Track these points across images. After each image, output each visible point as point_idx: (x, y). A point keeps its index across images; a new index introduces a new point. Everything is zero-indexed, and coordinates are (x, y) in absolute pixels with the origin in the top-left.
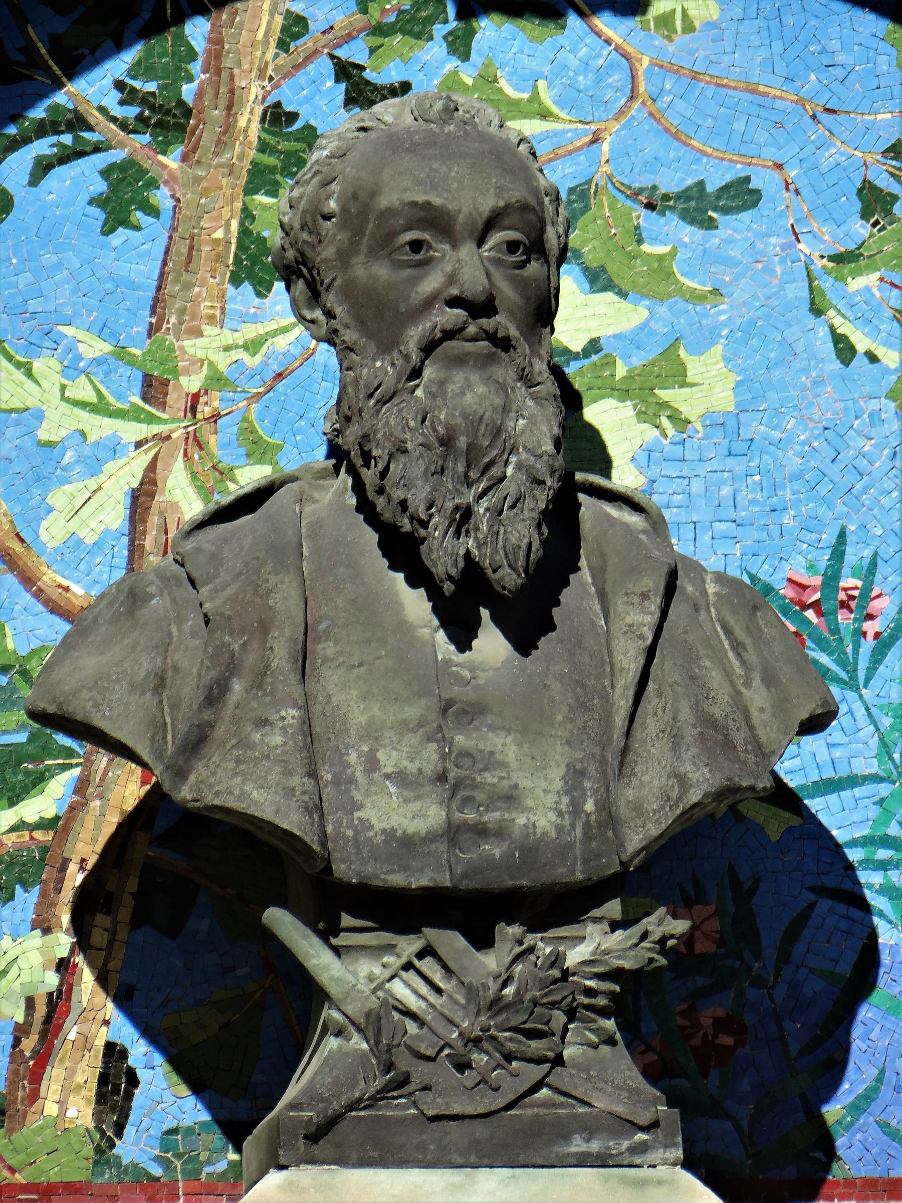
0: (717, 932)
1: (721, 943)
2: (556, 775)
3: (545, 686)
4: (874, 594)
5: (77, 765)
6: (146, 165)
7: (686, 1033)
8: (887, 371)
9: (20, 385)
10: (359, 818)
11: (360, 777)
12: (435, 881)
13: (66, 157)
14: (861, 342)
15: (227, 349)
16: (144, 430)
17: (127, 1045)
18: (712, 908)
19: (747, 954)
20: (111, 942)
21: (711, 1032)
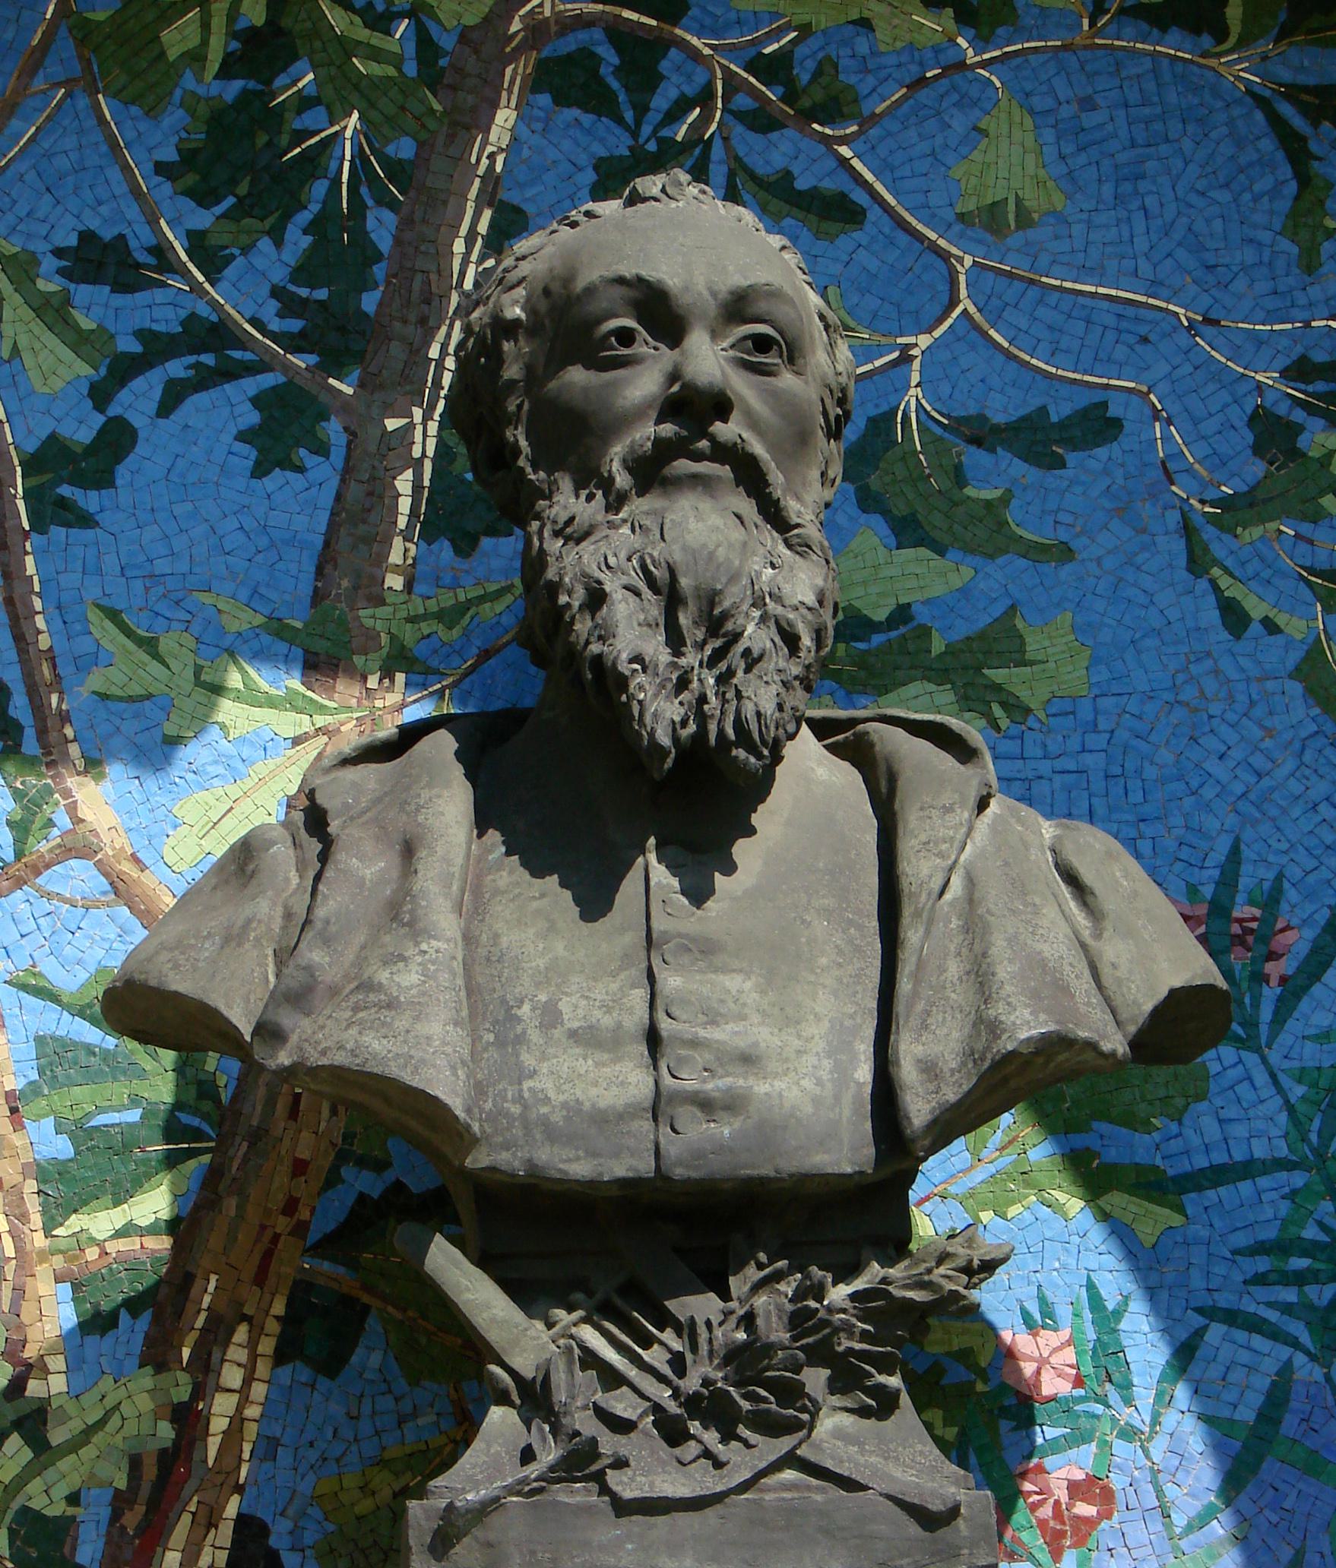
0: (1071, 1366)
1: (1079, 1382)
2: (817, 1032)
3: (803, 921)
4: (1279, 925)
5: (206, 1151)
6: (314, 390)
7: (1031, 1500)
8: (1290, 644)
9: (142, 666)
10: (530, 1089)
11: (535, 1036)
12: (636, 1170)
13: (204, 380)
14: (1256, 608)
15: (412, 620)
16: (304, 724)
17: (268, 1520)
18: (1065, 1334)
19: (1114, 1396)
20: (248, 1381)
21: (1064, 1498)
